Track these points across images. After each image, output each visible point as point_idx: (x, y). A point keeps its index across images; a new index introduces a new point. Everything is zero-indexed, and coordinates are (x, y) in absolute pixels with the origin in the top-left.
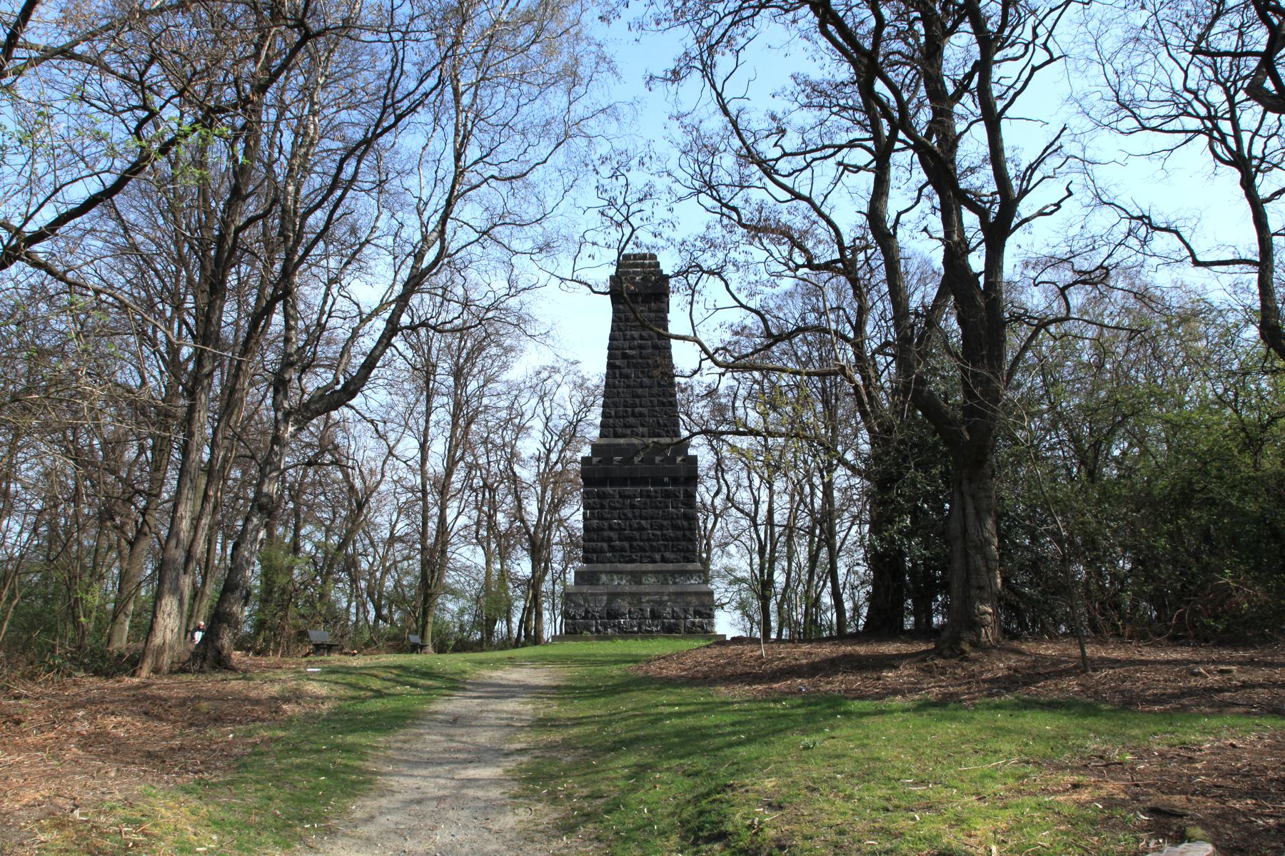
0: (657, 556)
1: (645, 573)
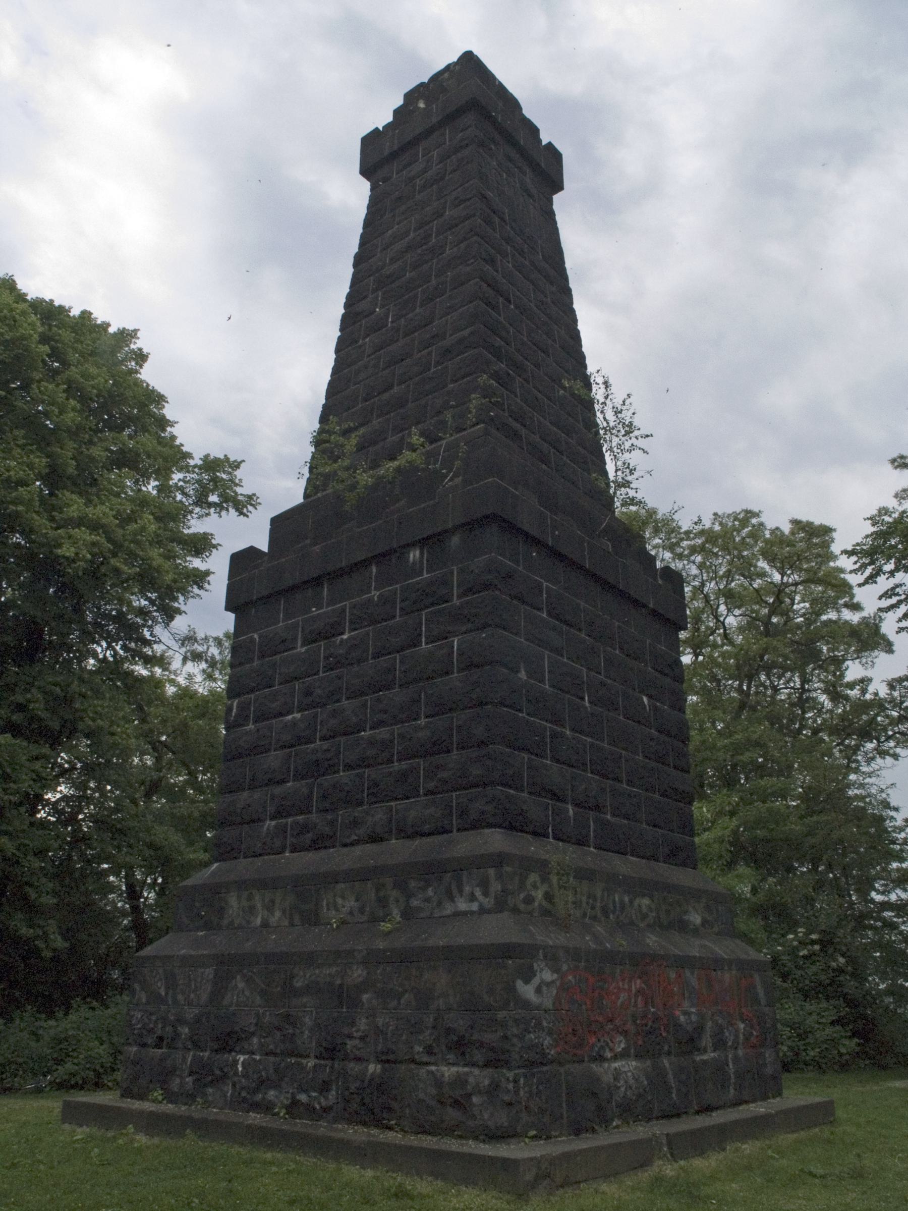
0: (377, 816)
1: (332, 878)
